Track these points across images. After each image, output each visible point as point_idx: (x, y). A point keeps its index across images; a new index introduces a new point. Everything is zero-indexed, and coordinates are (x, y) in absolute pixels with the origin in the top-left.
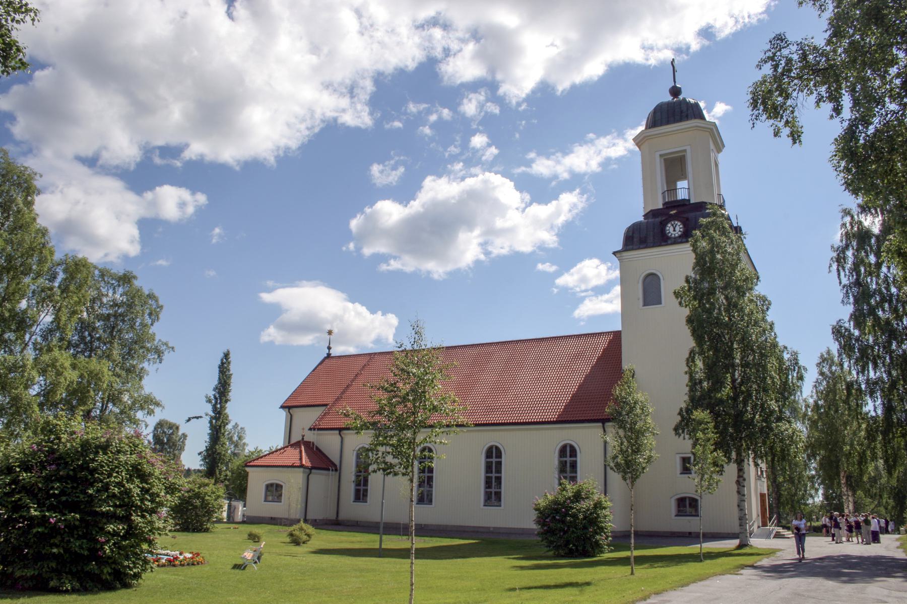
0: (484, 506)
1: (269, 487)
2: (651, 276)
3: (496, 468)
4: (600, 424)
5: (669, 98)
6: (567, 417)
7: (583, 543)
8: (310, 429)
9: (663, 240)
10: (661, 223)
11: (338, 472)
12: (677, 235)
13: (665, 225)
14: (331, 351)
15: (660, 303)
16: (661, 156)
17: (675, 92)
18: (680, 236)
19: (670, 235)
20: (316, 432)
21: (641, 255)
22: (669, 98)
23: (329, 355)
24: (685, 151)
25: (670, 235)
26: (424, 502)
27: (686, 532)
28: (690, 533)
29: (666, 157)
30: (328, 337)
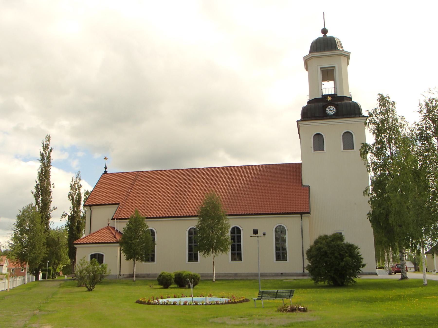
0: (231, 261)
1: (93, 256)
2: (347, 133)
3: (237, 239)
4: (300, 215)
5: (321, 35)
6: (287, 211)
7: (44, 302)
8: (113, 219)
9: (325, 116)
10: (323, 106)
11: (263, 235)
12: (332, 114)
13: (336, 107)
14: (107, 170)
15: (344, 149)
16: (321, 68)
17: (324, 31)
18: (334, 115)
19: (328, 113)
20: (118, 221)
21: (345, 121)
22: (321, 35)
23: (106, 172)
24: (335, 67)
25: (328, 113)
26: (192, 260)
27: (279, 273)
28: (282, 274)
29: (322, 69)
30: (104, 161)
